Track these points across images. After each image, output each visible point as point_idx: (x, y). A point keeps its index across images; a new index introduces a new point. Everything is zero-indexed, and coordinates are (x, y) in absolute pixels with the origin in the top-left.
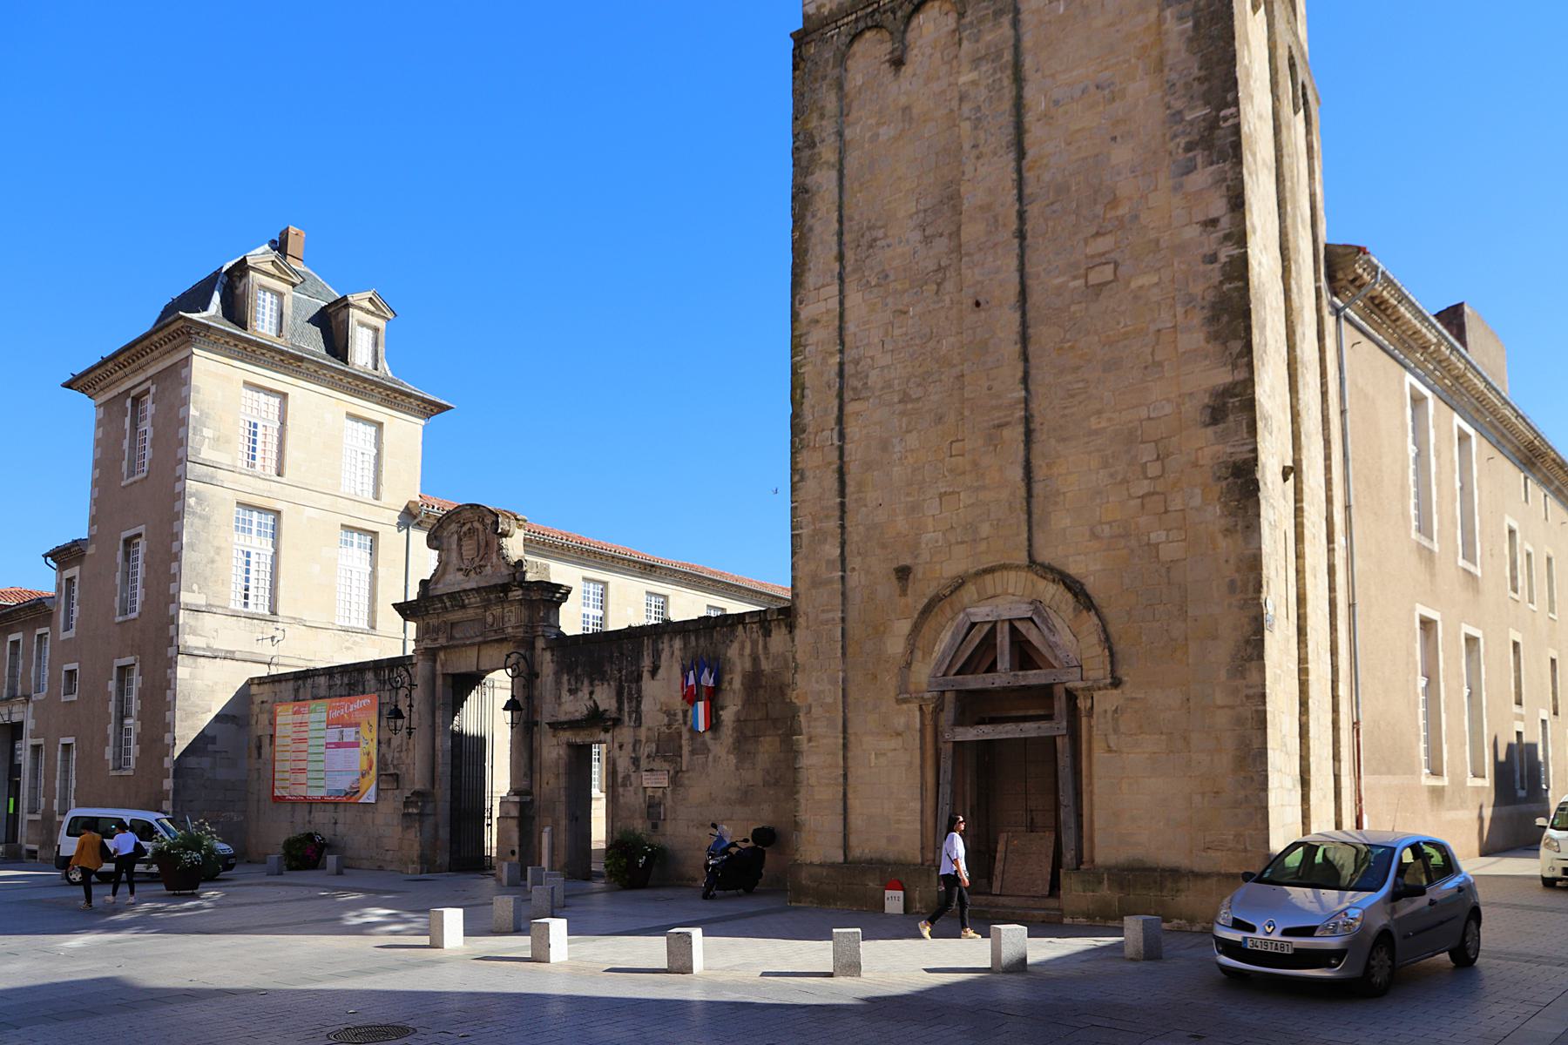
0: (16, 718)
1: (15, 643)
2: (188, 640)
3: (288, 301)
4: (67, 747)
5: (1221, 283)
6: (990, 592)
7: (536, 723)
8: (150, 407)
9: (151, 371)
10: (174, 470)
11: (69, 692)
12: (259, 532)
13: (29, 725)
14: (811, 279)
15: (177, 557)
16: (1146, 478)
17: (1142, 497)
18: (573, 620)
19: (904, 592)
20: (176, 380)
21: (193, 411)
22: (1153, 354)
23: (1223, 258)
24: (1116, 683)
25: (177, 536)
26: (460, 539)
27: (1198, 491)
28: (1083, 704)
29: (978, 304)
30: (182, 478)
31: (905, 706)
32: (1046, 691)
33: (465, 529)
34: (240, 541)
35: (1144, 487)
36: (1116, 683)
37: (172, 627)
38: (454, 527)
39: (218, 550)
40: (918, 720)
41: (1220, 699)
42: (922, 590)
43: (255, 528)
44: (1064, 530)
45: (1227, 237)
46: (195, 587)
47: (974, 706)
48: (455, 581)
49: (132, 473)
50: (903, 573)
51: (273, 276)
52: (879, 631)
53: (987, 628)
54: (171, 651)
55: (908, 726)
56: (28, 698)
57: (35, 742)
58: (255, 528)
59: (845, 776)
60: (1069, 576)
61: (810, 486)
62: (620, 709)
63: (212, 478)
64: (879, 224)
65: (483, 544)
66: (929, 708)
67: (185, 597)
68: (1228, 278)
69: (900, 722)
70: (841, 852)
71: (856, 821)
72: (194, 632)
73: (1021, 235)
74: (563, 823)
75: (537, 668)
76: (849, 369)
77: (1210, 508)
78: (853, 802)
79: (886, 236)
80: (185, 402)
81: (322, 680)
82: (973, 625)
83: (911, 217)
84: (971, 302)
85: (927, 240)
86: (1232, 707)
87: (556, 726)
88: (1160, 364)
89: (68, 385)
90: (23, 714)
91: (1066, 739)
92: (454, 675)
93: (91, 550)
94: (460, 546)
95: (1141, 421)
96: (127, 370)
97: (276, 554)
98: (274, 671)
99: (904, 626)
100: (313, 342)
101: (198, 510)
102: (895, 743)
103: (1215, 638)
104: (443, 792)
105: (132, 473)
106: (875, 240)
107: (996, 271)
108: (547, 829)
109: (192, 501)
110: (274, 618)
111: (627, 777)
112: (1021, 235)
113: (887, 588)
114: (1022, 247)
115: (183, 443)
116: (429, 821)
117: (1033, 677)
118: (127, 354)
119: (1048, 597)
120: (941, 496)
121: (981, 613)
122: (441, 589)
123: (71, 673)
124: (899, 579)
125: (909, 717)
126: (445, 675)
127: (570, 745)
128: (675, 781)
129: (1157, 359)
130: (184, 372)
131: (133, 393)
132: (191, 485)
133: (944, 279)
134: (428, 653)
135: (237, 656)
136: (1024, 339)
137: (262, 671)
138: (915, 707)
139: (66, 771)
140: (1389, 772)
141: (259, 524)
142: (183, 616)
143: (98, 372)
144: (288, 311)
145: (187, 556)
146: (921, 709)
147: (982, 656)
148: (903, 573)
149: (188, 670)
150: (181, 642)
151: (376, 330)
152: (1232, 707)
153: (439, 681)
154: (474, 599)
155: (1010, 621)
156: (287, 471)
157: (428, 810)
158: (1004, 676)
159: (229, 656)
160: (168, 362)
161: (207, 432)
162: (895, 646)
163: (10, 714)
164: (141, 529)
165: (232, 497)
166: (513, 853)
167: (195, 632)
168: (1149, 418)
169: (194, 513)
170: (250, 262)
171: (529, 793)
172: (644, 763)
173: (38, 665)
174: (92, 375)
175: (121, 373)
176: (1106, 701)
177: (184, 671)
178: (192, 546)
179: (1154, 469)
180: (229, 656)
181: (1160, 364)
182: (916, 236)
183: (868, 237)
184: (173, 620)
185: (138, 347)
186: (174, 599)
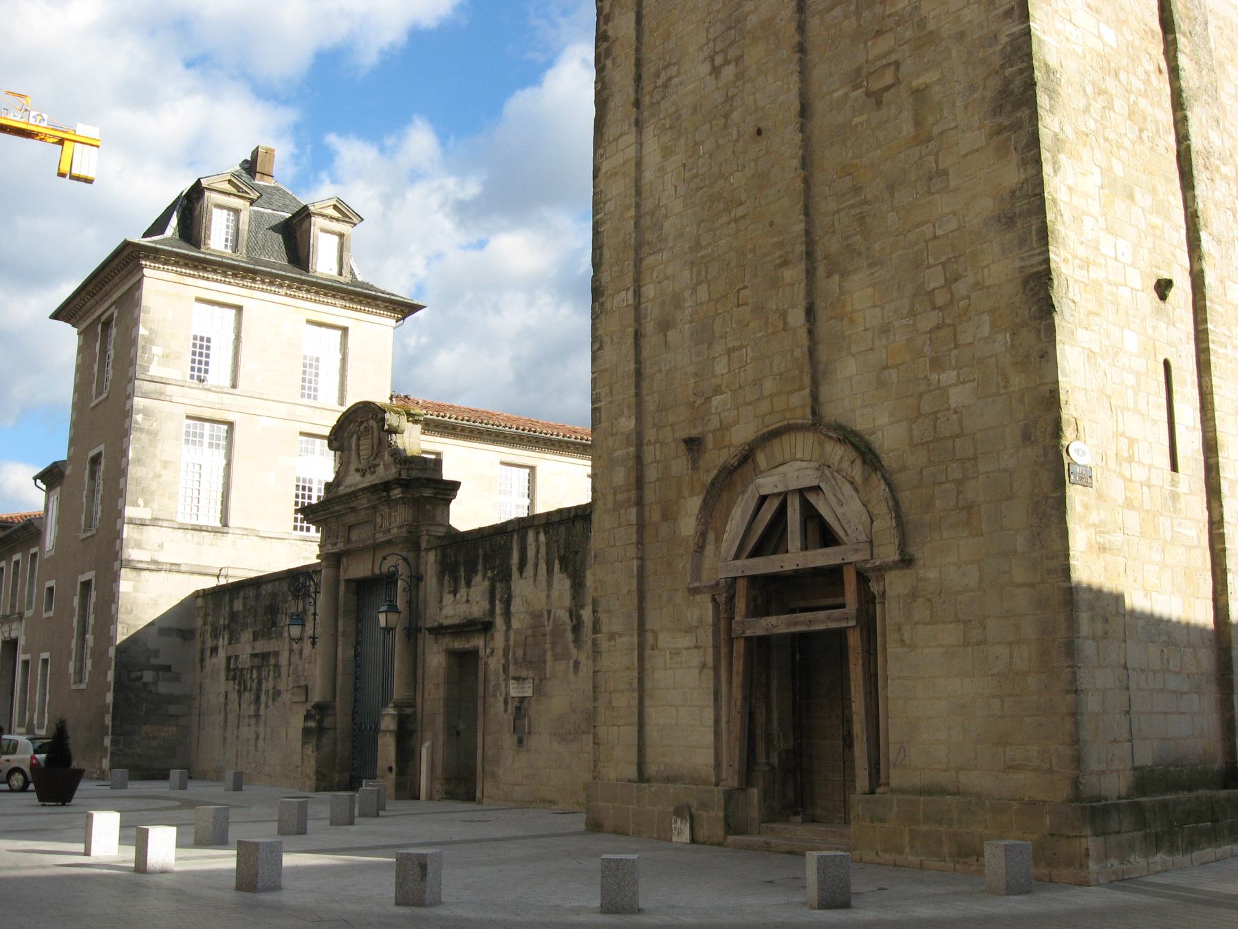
0: (13, 635)
1: (17, 563)
2: (132, 553)
3: (245, 217)
4: (45, 661)
5: (1002, 67)
6: (779, 459)
7: (419, 630)
8: (114, 331)
9: (115, 296)
10: (125, 388)
11: (49, 609)
12: (211, 445)
13: (22, 642)
14: (610, 132)
15: (123, 473)
16: (934, 308)
17: (930, 332)
18: (467, 514)
19: (695, 468)
20: (131, 300)
21: (142, 331)
22: (936, 163)
23: (1004, 39)
24: (906, 561)
25: (124, 453)
26: (358, 439)
27: (986, 317)
28: (874, 587)
29: (759, 132)
30: (130, 397)
31: (698, 597)
32: (833, 574)
33: (362, 428)
34: (188, 455)
35: (932, 319)
36: (906, 561)
37: (118, 541)
38: (352, 427)
39: (166, 464)
40: (710, 613)
41: (1019, 577)
42: (716, 459)
43: (206, 440)
44: (851, 378)
45: (1008, 13)
46: (141, 501)
47: (773, 592)
48: (354, 480)
49: (99, 393)
50: (693, 444)
51: (229, 194)
52: (669, 515)
53: (776, 503)
54: (117, 564)
55: (700, 620)
56: (21, 616)
57: (28, 657)
58: (206, 440)
59: (641, 680)
60: (855, 434)
61: (608, 354)
62: (492, 611)
63: (162, 394)
64: (674, 60)
65: (376, 441)
66: (722, 599)
67: (130, 512)
68: (1008, 59)
69: (692, 615)
70: (635, 768)
71: (652, 734)
72: (138, 545)
73: (801, 49)
74: (441, 737)
75: (422, 569)
76: (647, 221)
77: (1000, 337)
78: (650, 711)
79: (679, 74)
80: (135, 323)
81: (251, 593)
82: (763, 499)
83: (701, 49)
84: (753, 130)
85: (716, 71)
86: (1032, 586)
87: (439, 631)
88: (945, 173)
89: (56, 316)
90: (18, 632)
91: (858, 632)
92: (749, 577)
93: (68, 471)
94: (358, 446)
95: (926, 241)
96: (97, 298)
97: (228, 465)
98: (223, 581)
99: (694, 504)
100: (275, 255)
101: (146, 426)
102: (685, 641)
103: (1010, 498)
104: (342, 706)
105: (99, 393)
106: (669, 79)
107: (775, 92)
108: (427, 744)
109: (139, 418)
110: (225, 529)
111: (497, 686)
112: (801, 49)
113: (680, 465)
114: (802, 63)
115: (132, 362)
116: (327, 739)
117: (822, 558)
118: (94, 282)
119: (837, 458)
120: (729, 352)
121: (768, 484)
122: (342, 490)
123: (51, 590)
124: (690, 450)
125: (703, 610)
126: (348, 581)
127: (451, 653)
128: (538, 691)
129: (941, 166)
130: (137, 294)
131: (103, 318)
132: (138, 402)
133: (732, 110)
134: (331, 558)
135: (183, 568)
136: (806, 163)
137: (210, 583)
138: (707, 598)
139: (44, 686)
140: (545, 662)
141: (211, 437)
142: (127, 531)
143: (75, 301)
144: (244, 226)
145: (133, 471)
146: (714, 600)
147: (771, 539)
148: (693, 444)
149: (132, 583)
150: (125, 556)
151: (341, 236)
152: (1032, 586)
153: (342, 588)
154: (363, 502)
155: (801, 492)
156: (241, 382)
157: (327, 723)
158: (796, 557)
159: (175, 568)
160: (126, 287)
161: (156, 350)
162: (688, 525)
163: (10, 630)
164: (101, 448)
165: (182, 411)
166: (390, 769)
167: (138, 544)
168: (935, 238)
169: (141, 430)
170: (204, 183)
171: (412, 705)
172: (512, 671)
173: (31, 584)
174: (71, 306)
175: (92, 302)
176: (896, 585)
177: (127, 585)
178: (138, 461)
179: (941, 299)
180: (175, 568)
181: (945, 173)
182: (706, 68)
183: (663, 77)
184: (118, 534)
185: (102, 275)
186: (120, 514)
